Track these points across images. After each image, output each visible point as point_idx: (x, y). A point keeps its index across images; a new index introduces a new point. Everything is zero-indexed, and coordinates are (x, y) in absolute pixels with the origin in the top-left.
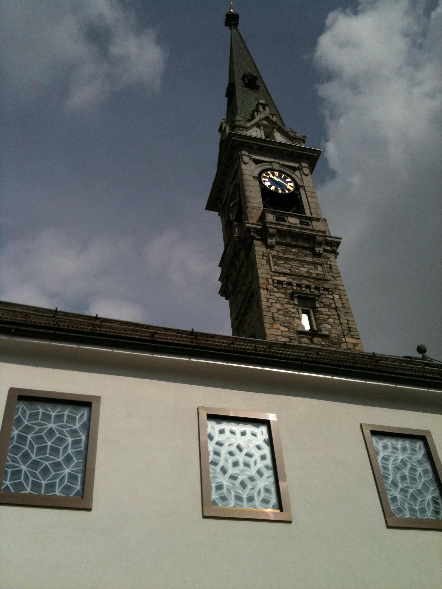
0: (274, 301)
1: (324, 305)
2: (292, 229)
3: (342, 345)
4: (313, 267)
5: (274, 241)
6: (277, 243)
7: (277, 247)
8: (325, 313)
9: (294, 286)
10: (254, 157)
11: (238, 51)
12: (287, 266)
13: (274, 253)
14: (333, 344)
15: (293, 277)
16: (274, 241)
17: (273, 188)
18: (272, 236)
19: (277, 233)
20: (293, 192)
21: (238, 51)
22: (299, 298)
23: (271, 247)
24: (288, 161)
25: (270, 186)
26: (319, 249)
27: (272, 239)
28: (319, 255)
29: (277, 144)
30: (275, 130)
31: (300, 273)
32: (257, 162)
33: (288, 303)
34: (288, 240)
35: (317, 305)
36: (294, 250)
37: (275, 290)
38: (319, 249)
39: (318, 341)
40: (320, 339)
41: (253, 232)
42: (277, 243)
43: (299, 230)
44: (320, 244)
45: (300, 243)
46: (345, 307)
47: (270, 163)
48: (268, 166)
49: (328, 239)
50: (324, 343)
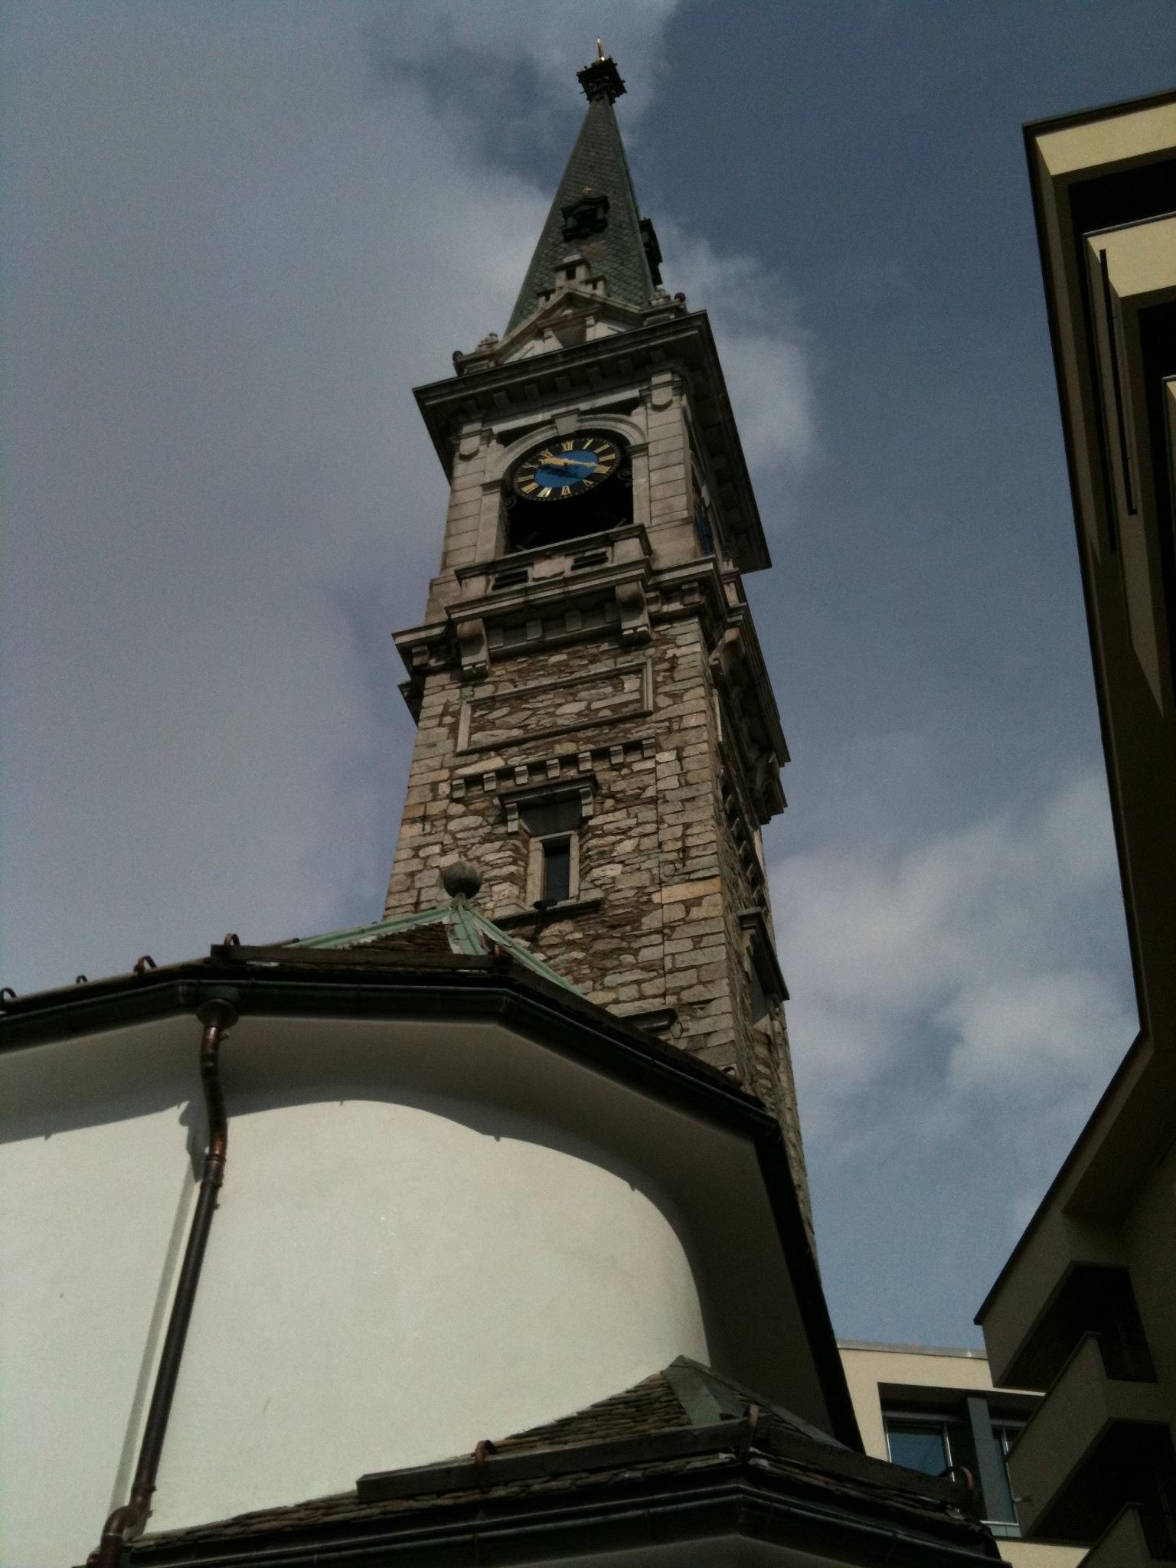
0: (437, 849)
1: (618, 801)
2: (531, 597)
3: (644, 920)
4: (609, 689)
5: (483, 655)
6: (495, 659)
7: (499, 671)
8: (611, 827)
9: (521, 774)
10: (497, 428)
11: (598, 144)
12: (514, 719)
13: (484, 692)
14: (613, 927)
15: (525, 746)
16: (483, 655)
17: (566, 491)
18: (473, 642)
19: (488, 628)
20: (612, 478)
21: (598, 144)
22: (524, 809)
23: (477, 677)
24: (612, 390)
25: (556, 491)
26: (639, 623)
27: (476, 652)
28: (640, 641)
29: (561, 359)
30: (590, 321)
31: (554, 725)
32: (506, 439)
33: (487, 839)
34: (534, 635)
35: (587, 811)
36: (555, 659)
37: (459, 808)
38: (639, 623)
39: (561, 935)
40: (566, 926)
41: (418, 654)
42: (495, 659)
43: (557, 591)
44: (634, 605)
45: (575, 628)
46: (688, 784)
47: (551, 422)
48: (539, 437)
49: (667, 577)
50: (578, 935)
